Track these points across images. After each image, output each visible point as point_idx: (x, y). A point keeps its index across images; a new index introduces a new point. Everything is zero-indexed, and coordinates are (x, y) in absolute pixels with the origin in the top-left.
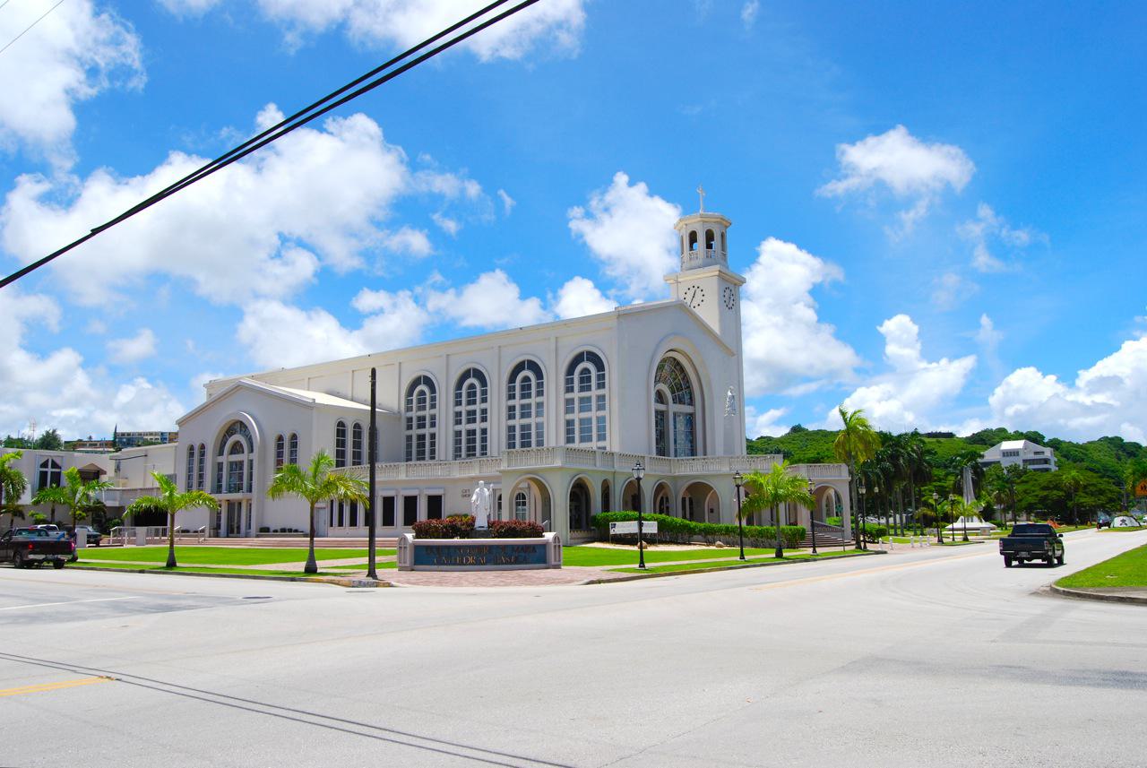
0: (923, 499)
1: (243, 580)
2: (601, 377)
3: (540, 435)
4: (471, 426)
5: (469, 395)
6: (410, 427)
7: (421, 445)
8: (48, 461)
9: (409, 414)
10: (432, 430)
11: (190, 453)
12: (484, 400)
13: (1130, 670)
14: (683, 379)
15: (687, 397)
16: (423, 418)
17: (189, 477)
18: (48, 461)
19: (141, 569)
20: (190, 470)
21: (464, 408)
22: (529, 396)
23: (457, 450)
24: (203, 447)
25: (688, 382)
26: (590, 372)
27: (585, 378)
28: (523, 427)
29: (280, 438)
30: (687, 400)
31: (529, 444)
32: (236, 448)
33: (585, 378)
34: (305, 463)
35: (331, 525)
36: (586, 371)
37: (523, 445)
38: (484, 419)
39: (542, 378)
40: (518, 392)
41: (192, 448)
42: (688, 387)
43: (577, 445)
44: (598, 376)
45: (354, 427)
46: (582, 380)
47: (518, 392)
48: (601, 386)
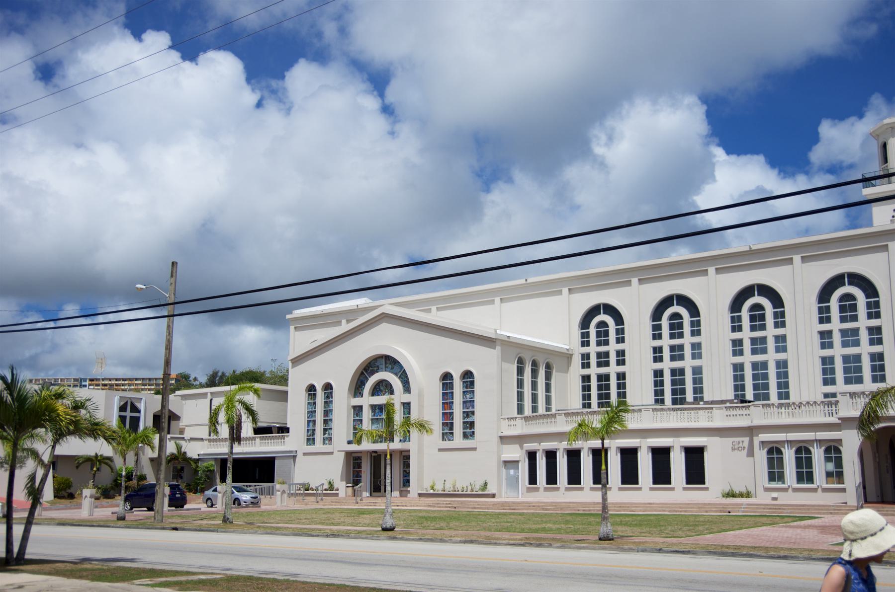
0: (98, 463)
2: (620, 332)
3: (698, 381)
8: (126, 403)
13: (463, 545)
17: (311, 422)
18: (126, 403)
19: (173, 526)
20: (312, 413)
23: (659, 394)
24: (328, 387)
27: (848, 307)
28: (600, 378)
32: (382, 387)
33: (848, 307)
34: (141, 427)
35: (474, 449)
39: (782, 306)
40: (593, 338)
44: (692, 322)
46: (598, 334)
47: (593, 338)
48: (696, 333)
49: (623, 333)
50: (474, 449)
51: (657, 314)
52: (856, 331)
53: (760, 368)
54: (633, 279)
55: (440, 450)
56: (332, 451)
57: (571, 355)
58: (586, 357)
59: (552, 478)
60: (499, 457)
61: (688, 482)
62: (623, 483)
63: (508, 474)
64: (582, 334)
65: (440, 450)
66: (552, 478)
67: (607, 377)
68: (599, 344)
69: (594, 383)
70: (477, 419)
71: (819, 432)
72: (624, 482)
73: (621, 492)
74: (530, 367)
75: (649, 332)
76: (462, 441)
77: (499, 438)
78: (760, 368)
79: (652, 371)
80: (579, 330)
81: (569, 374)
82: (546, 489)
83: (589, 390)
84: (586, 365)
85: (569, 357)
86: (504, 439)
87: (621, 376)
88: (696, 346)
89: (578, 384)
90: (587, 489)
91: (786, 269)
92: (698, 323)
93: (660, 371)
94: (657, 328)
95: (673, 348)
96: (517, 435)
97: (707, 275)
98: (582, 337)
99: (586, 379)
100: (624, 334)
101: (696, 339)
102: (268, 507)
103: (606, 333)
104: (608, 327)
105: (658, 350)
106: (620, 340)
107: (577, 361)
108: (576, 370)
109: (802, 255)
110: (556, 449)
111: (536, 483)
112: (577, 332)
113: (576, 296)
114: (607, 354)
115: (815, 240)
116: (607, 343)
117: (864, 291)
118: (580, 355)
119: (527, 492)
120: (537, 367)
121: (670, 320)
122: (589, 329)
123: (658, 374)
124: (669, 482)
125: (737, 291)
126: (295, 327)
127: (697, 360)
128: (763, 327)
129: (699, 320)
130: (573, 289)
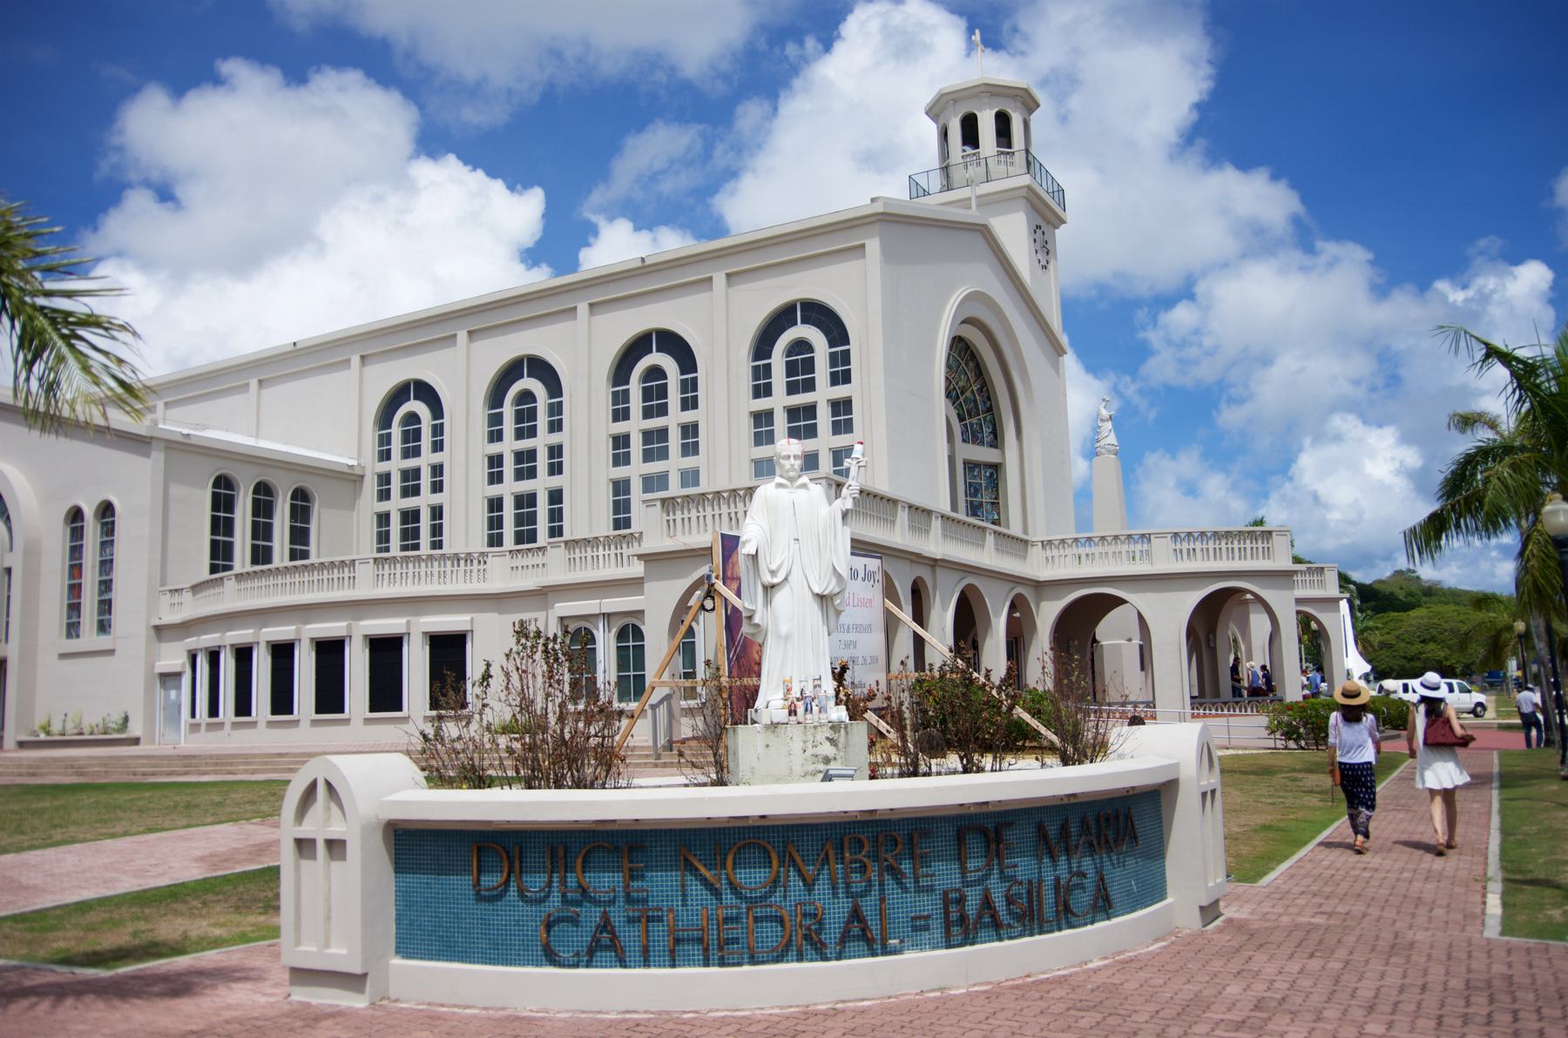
1: (334, 725)
2: (689, 386)
4: (410, 503)
5: (406, 436)
6: (384, 495)
7: (526, 519)
9: (384, 467)
10: (436, 499)
11: (74, 530)
12: (438, 446)
14: (980, 390)
15: (987, 430)
16: (531, 455)
21: (509, 446)
22: (532, 432)
25: (989, 398)
26: (810, 349)
29: (76, 515)
30: (988, 438)
31: (532, 537)
35: (111, 652)
36: (802, 346)
37: (520, 538)
38: (437, 487)
39: (846, 341)
41: (76, 515)
42: (990, 410)
43: (962, 516)
45: (294, 497)
46: (791, 369)
47: (779, 378)
49: (695, 388)
50: (111, 652)
51: (621, 372)
52: (810, 410)
53: (526, 501)
54: (714, 275)
55: (63, 656)
56: (111, 647)
57: (362, 477)
58: (385, 479)
59: (282, 701)
60: (150, 665)
61: (374, 707)
62: (373, 709)
63: (167, 697)
64: (756, 369)
65: (63, 656)
66: (282, 701)
67: (531, 499)
68: (648, 413)
69: (395, 527)
70: (118, 596)
71: (205, 634)
72: (320, 709)
73: (1567, 762)
74: (288, 501)
75: (746, 382)
76: (95, 637)
77: (152, 633)
78: (526, 501)
79: (546, 492)
80: (374, 431)
81: (355, 513)
82: (235, 725)
83: (500, 526)
84: (384, 495)
85: (353, 479)
86: (161, 632)
87: (556, 496)
88: (690, 430)
89: (369, 530)
90: (262, 725)
91: (443, 355)
92: (846, 357)
93: (497, 499)
94: (621, 398)
95: (648, 436)
96: (179, 621)
97: (864, 256)
98: (756, 377)
99: (384, 519)
100: (628, 402)
101: (841, 391)
102: (1342, 820)
103: (809, 366)
104: (813, 351)
105: (621, 441)
106: (555, 426)
107: (370, 487)
108: (369, 504)
109: (728, 271)
110: (219, 647)
111: (249, 713)
112: (371, 435)
113: (374, 370)
114: (810, 410)
115: (589, 277)
116: (810, 386)
117: (827, 332)
118: (486, 459)
119: (312, 726)
120: (308, 501)
121: (644, 382)
122: (628, 383)
123: (495, 504)
124: (340, 709)
125: (767, 313)
126: (728, 275)
127: (622, 468)
128: (810, 386)
129: (848, 351)
130: (268, 379)
